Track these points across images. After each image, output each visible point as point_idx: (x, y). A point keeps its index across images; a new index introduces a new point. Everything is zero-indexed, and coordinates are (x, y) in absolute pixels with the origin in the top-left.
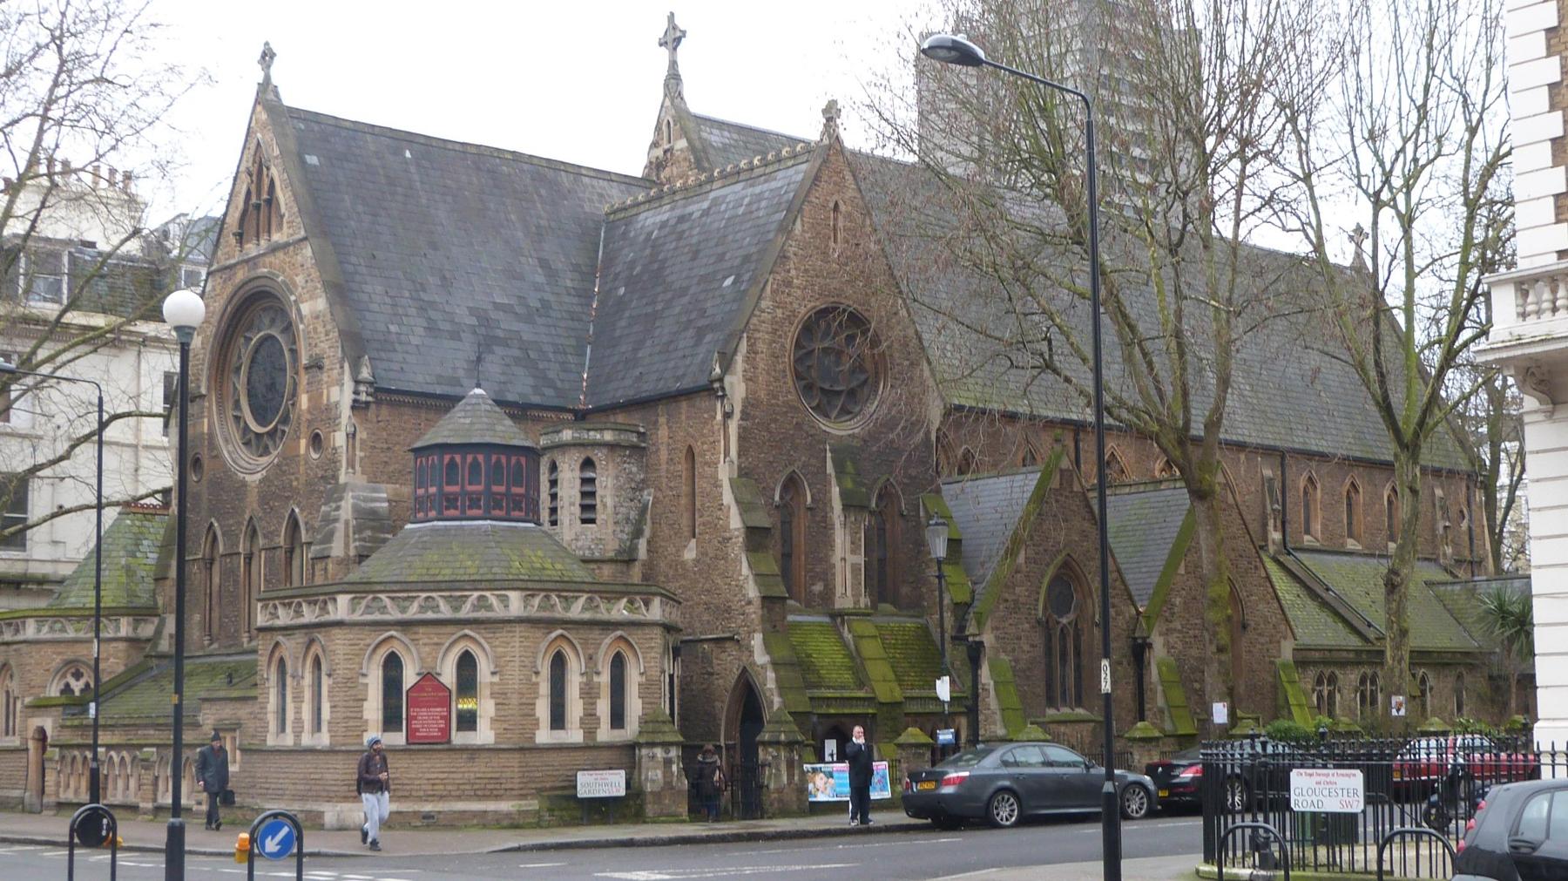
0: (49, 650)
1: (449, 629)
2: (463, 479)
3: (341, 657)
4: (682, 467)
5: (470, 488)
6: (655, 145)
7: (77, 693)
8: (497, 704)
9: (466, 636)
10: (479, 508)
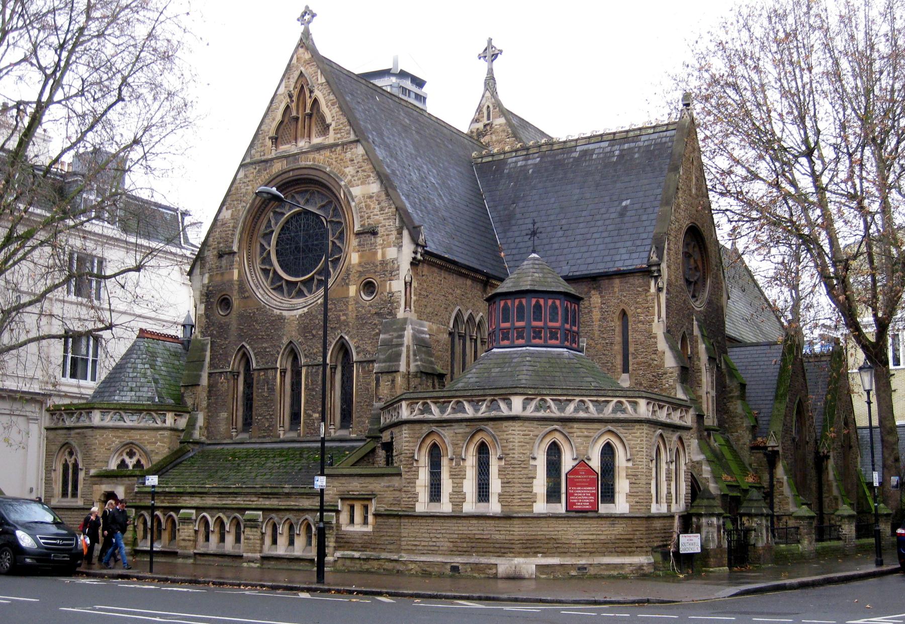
0: (110, 434)
1: (596, 426)
2: (545, 318)
3: (517, 444)
4: (617, 324)
5: (551, 324)
6: (476, 121)
7: (131, 467)
8: (502, 483)
10: (557, 339)
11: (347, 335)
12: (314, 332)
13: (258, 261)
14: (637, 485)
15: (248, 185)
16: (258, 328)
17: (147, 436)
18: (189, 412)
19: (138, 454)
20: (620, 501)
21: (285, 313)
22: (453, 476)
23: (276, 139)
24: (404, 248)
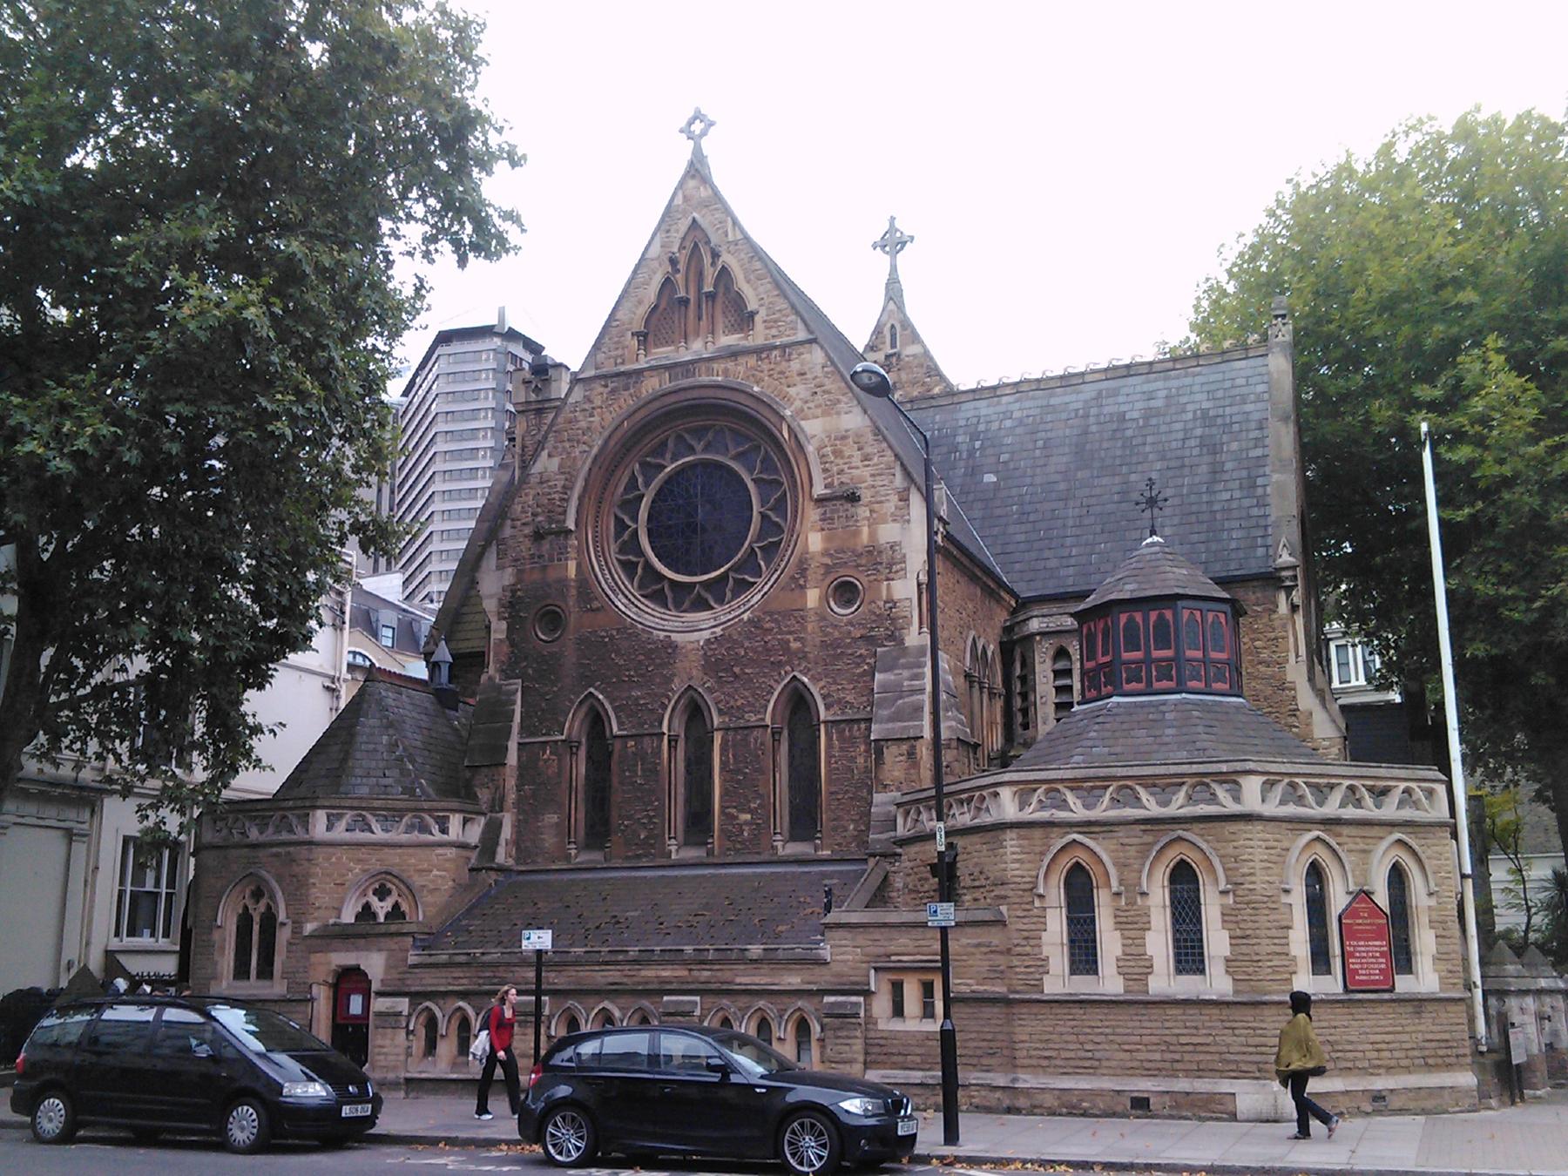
0: (344, 855)
3: (1258, 865)
9: (1180, 839)
11: (805, 675)
12: (736, 670)
13: (614, 547)
14: (1447, 941)
15: (592, 415)
16: (622, 662)
17: (413, 859)
18: (484, 814)
19: (395, 893)
20: (1426, 970)
21: (674, 636)
22: (1120, 924)
23: (646, 335)
24: (913, 525)
